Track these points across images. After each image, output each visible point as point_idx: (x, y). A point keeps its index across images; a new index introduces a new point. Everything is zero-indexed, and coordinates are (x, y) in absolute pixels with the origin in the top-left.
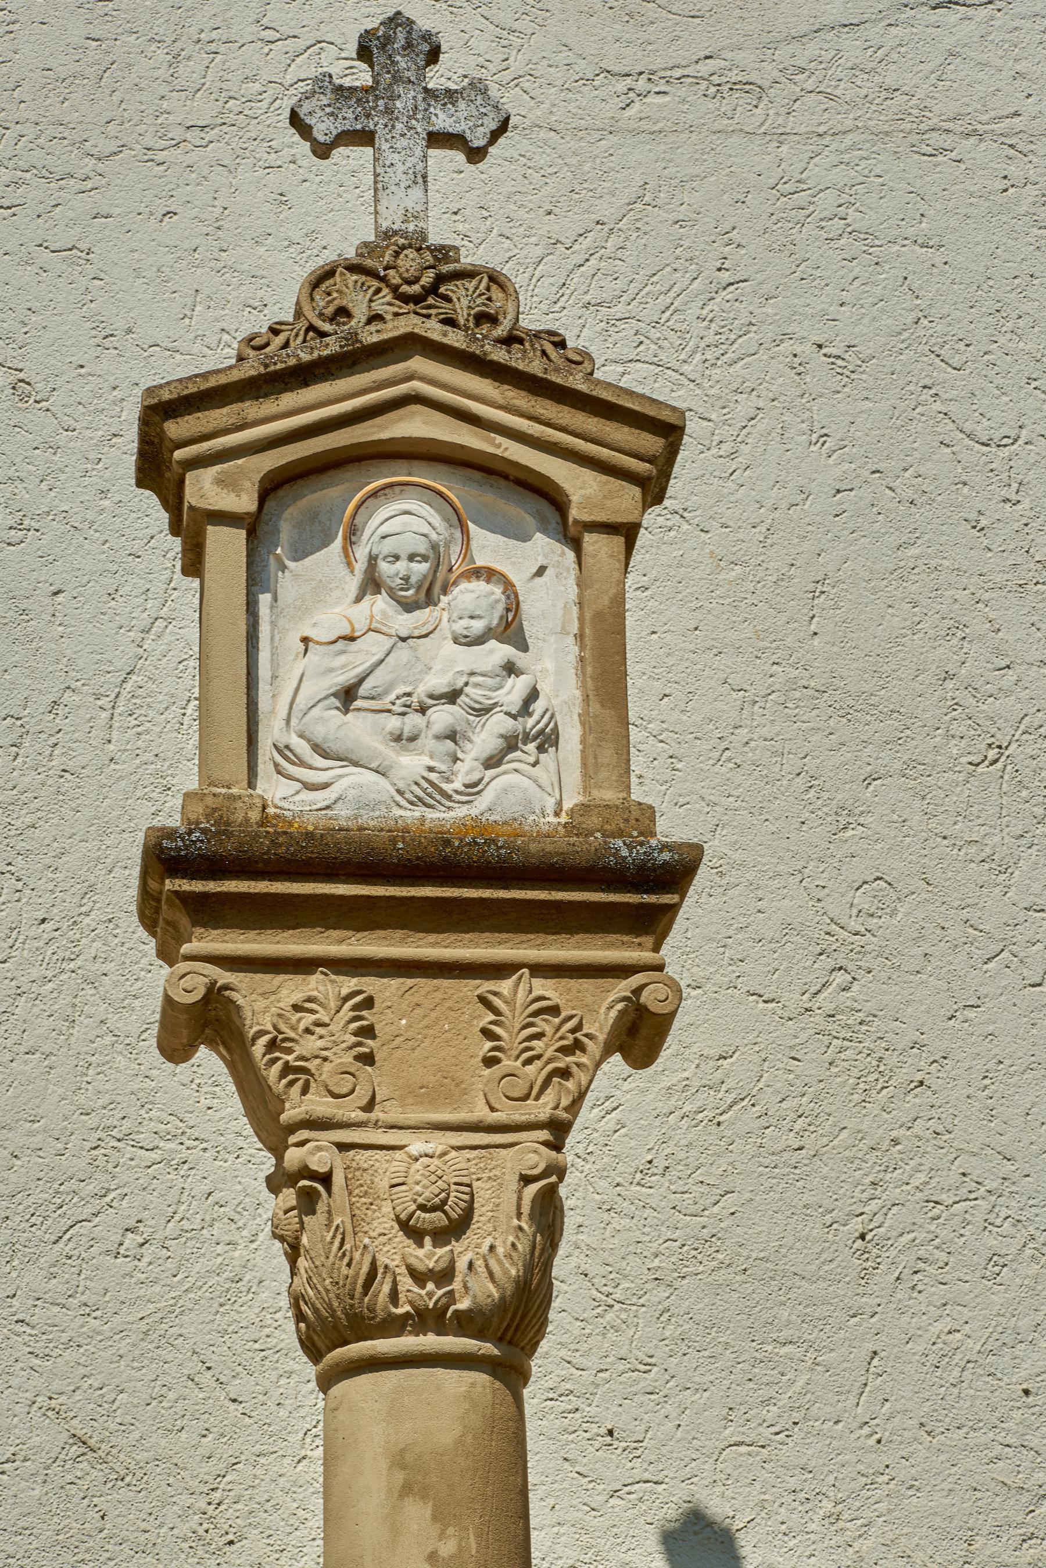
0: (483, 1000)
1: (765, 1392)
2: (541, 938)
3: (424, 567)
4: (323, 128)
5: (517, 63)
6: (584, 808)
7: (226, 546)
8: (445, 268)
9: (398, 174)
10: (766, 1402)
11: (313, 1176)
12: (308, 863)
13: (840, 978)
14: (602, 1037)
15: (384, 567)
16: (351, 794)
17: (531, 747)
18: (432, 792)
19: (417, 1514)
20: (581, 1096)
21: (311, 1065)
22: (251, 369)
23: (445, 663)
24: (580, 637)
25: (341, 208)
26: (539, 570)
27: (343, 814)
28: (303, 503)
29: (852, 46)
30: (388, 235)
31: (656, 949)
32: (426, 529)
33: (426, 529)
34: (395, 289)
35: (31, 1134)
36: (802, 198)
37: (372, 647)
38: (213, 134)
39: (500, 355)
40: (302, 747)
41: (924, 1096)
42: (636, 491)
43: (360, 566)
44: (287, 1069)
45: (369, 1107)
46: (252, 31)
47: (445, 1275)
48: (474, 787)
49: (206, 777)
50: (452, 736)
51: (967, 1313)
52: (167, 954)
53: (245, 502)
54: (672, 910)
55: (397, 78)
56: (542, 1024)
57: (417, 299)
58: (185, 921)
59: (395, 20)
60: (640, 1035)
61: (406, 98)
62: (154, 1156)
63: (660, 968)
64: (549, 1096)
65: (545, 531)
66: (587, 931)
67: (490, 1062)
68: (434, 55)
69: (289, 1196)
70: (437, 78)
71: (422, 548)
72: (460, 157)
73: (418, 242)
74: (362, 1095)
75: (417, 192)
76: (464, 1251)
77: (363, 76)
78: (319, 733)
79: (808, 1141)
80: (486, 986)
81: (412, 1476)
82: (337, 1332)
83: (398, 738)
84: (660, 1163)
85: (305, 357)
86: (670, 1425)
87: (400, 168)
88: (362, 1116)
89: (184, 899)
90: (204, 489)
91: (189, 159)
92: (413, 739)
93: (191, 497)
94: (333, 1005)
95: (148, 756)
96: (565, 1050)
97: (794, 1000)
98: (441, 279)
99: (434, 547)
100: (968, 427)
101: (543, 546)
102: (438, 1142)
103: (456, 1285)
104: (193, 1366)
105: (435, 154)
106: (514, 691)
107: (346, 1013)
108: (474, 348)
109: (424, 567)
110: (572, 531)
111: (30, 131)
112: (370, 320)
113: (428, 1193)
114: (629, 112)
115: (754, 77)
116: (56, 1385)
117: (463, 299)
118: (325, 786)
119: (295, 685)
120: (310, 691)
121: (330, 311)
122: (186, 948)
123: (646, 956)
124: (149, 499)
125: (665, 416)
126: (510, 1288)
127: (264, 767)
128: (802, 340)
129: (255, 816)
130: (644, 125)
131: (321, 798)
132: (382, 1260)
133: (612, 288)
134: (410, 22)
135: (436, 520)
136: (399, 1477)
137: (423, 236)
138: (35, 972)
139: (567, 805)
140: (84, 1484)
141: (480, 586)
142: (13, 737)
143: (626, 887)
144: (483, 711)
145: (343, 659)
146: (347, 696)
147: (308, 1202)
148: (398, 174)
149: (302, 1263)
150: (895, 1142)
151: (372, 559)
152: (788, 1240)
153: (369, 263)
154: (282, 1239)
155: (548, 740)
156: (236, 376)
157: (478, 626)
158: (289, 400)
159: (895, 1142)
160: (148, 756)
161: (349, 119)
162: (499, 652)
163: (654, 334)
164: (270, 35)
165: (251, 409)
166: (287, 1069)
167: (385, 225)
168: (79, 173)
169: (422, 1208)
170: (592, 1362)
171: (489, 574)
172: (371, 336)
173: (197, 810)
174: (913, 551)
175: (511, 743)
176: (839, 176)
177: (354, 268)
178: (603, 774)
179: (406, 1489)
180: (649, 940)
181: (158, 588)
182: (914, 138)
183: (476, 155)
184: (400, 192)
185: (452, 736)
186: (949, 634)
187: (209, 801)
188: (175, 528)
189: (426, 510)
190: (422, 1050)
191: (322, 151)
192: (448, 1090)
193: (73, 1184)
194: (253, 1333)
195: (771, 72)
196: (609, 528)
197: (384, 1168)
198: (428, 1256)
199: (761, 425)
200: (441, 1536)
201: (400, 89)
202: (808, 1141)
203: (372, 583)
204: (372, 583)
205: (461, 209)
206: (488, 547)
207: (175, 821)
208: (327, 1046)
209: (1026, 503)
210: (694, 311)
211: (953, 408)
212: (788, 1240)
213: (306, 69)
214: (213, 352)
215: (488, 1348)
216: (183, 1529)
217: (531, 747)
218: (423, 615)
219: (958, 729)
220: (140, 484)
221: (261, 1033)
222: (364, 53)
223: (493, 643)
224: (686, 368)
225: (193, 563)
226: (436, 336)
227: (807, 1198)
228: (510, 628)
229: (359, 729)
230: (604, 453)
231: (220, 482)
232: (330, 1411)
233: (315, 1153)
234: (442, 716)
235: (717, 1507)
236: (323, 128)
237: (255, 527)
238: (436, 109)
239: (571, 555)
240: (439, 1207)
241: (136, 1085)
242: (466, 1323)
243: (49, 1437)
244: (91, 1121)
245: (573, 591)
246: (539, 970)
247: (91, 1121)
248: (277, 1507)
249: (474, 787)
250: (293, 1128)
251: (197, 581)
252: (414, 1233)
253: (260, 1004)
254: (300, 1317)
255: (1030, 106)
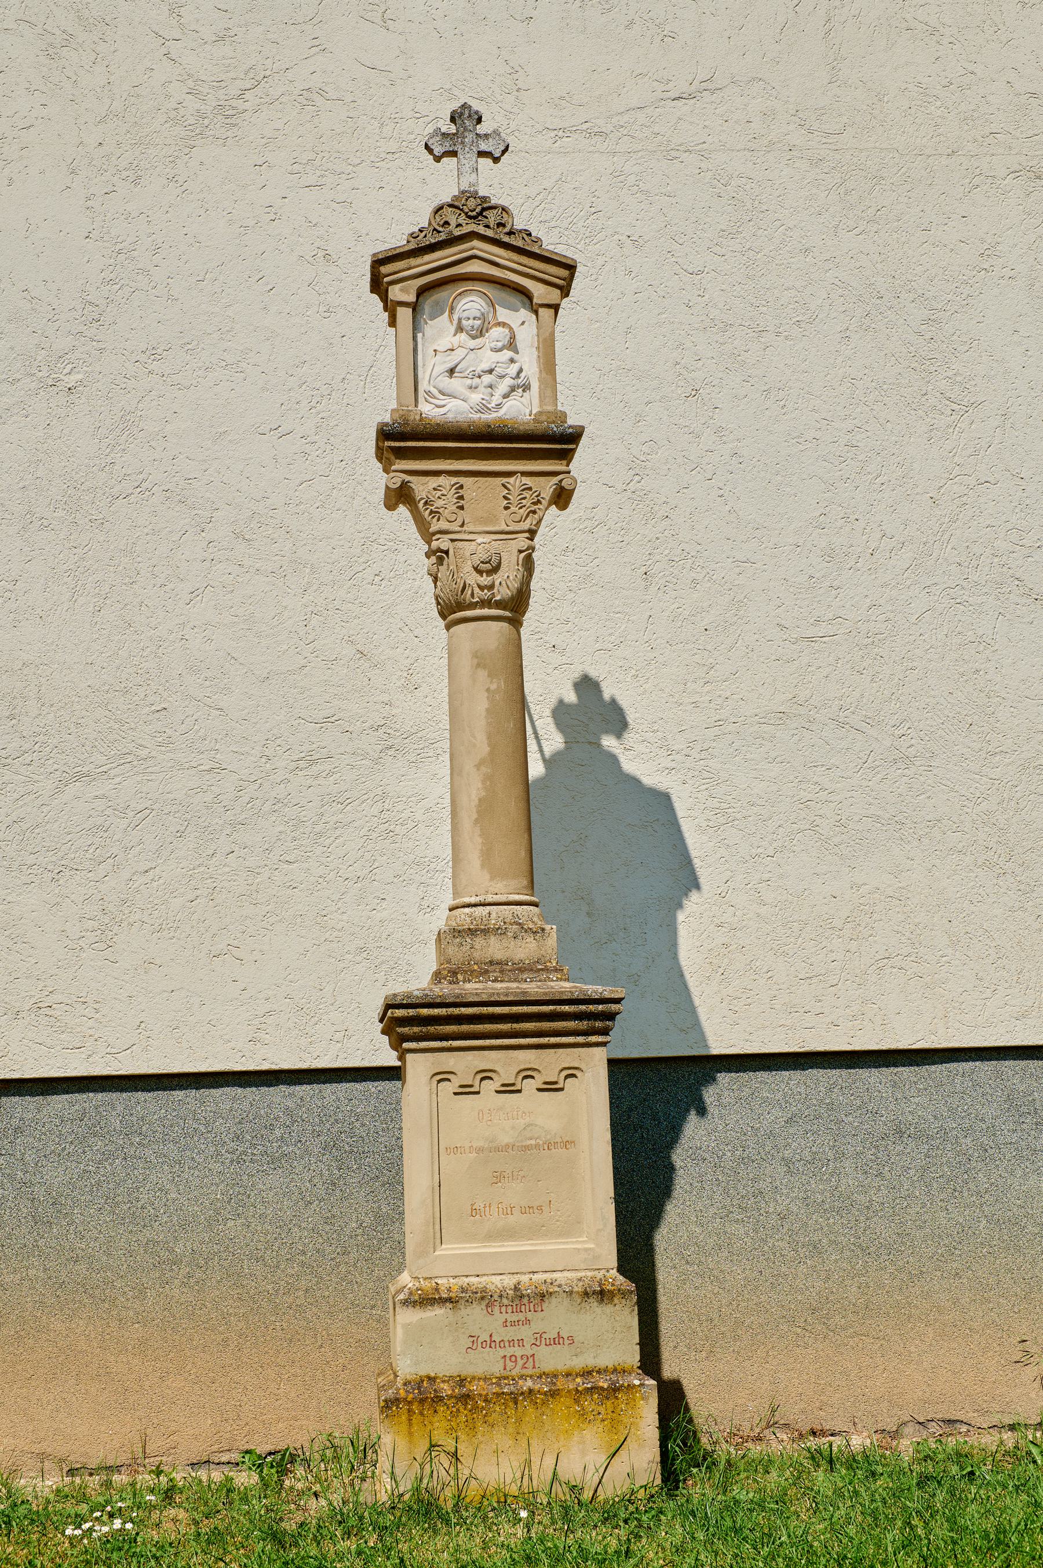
0: (503, 485)
1: (610, 631)
2: (525, 462)
3: (479, 322)
4: (438, 150)
5: (513, 126)
6: (540, 413)
7: (404, 315)
8: (485, 205)
9: (467, 168)
10: (611, 635)
11: (442, 551)
12: (438, 434)
13: (637, 478)
14: (548, 499)
15: (464, 322)
16: (454, 409)
17: (520, 390)
18: (484, 408)
19: (482, 674)
20: (540, 520)
21: (440, 510)
22: (412, 246)
23: (487, 359)
24: (538, 348)
25: (445, 182)
26: (520, 320)
27: (450, 417)
28: (433, 298)
29: (641, 116)
30: (463, 192)
31: (568, 465)
32: (479, 307)
33: (479, 307)
34: (466, 214)
35: (340, 540)
36: (622, 178)
37: (460, 353)
38: (397, 156)
39: (506, 239)
40: (435, 392)
41: (668, 522)
42: (559, 292)
43: (455, 322)
44: (432, 512)
45: (462, 525)
46: (411, 114)
47: (491, 587)
48: (499, 406)
49: (400, 404)
50: (491, 387)
51: (684, 601)
52: (386, 471)
53: (411, 298)
54: (573, 451)
55: (465, 129)
56: (526, 494)
57: (474, 218)
58: (393, 458)
59: (464, 106)
60: (562, 498)
61: (469, 137)
62: (385, 547)
63: (569, 472)
64: (528, 521)
65: (524, 308)
66: (542, 459)
67: (506, 508)
68: (479, 120)
69: (433, 559)
70: (481, 129)
71: (478, 315)
72: (489, 161)
73: (474, 195)
74: (459, 522)
75: (474, 175)
76: (498, 578)
77: (453, 129)
78: (441, 386)
79: (626, 538)
80: (504, 480)
81: (480, 661)
82: (452, 609)
83: (471, 388)
84: (571, 547)
85: (433, 241)
86: (576, 643)
87: (467, 166)
88: (460, 529)
89: (393, 449)
90: (396, 293)
91: (388, 166)
92: (476, 388)
93: (391, 296)
94: (448, 488)
95: (379, 398)
96: (534, 503)
97: (620, 486)
98: (484, 209)
99: (483, 314)
100: (685, 267)
101: (524, 314)
102: (488, 538)
103: (495, 591)
104: (401, 624)
105: (481, 160)
106: (513, 369)
107: (453, 491)
108: (497, 237)
109: (479, 322)
110: (535, 307)
111: (327, 155)
112: (457, 226)
113: (484, 557)
114: (556, 145)
115: (604, 130)
116: (351, 632)
117: (492, 217)
118: (444, 406)
119: (432, 368)
120: (438, 369)
121: (442, 223)
122: (393, 468)
123: (564, 468)
124: (375, 297)
125: (569, 262)
126: (515, 592)
127: (421, 399)
128: (622, 234)
129: (418, 417)
130: (562, 150)
131: (442, 410)
132: (468, 582)
133: (550, 215)
134: (470, 107)
135: (483, 304)
136: (476, 661)
137: (476, 192)
138: (339, 480)
139: (534, 412)
140: (362, 668)
141: (500, 329)
142: (328, 392)
143: (558, 442)
144: (502, 377)
145: (449, 358)
146: (452, 371)
147: (440, 561)
148: (467, 168)
149: (438, 583)
150: (657, 538)
151: (460, 319)
152: (619, 575)
153: (456, 203)
154: (431, 575)
155: (526, 387)
156: (406, 248)
157: (500, 344)
158: (427, 258)
159: (657, 538)
160: (379, 398)
161: (447, 146)
162: (508, 354)
163: (566, 233)
164: (418, 115)
165: (413, 261)
166: (432, 512)
167: (462, 189)
168: (347, 172)
169: (482, 562)
170: (547, 621)
171: (504, 324)
172: (457, 232)
173: (396, 416)
174: (664, 316)
175: (513, 389)
176: (636, 169)
177: (451, 206)
178: (547, 400)
179: (478, 665)
180: (565, 462)
181: (381, 334)
182: (665, 153)
183: (496, 160)
184: (468, 175)
185: (491, 387)
186: (678, 347)
187: (401, 412)
188: (386, 309)
189: (479, 300)
190: (482, 503)
191: (438, 159)
192: (492, 519)
193: (355, 558)
194: (422, 612)
195: (610, 127)
196: (548, 306)
197: (469, 547)
198: (485, 580)
199: (607, 268)
200: (491, 682)
201: (466, 134)
202: (626, 538)
203: (460, 329)
204: (460, 329)
205: (492, 182)
206: (503, 314)
207: (387, 419)
208: (447, 503)
209: (707, 296)
210: (581, 224)
211: (679, 260)
212: (619, 575)
213: (430, 129)
214: (397, 239)
215: (507, 614)
216: (399, 684)
217: (520, 390)
218: (479, 341)
219: (681, 383)
220: (372, 292)
221: (422, 499)
222: (453, 119)
223: (505, 351)
224: (578, 246)
225: (393, 322)
226: (482, 232)
227: (626, 559)
228: (511, 345)
229: (456, 384)
230: (546, 277)
231: (401, 290)
232: (450, 638)
233: (443, 543)
234: (487, 379)
235: (593, 674)
236: (438, 150)
237: (415, 307)
238: (481, 142)
239: (534, 317)
240: (489, 562)
241: (377, 521)
242: (499, 605)
243: (349, 651)
244: (362, 535)
245: (535, 331)
246: (524, 474)
247: (362, 535)
248: (433, 675)
249: (499, 406)
250: (434, 534)
251: (547, 754)
252: (480, 572)
253: (421, 488)
254: (438, 603)
255: (710, 139)
